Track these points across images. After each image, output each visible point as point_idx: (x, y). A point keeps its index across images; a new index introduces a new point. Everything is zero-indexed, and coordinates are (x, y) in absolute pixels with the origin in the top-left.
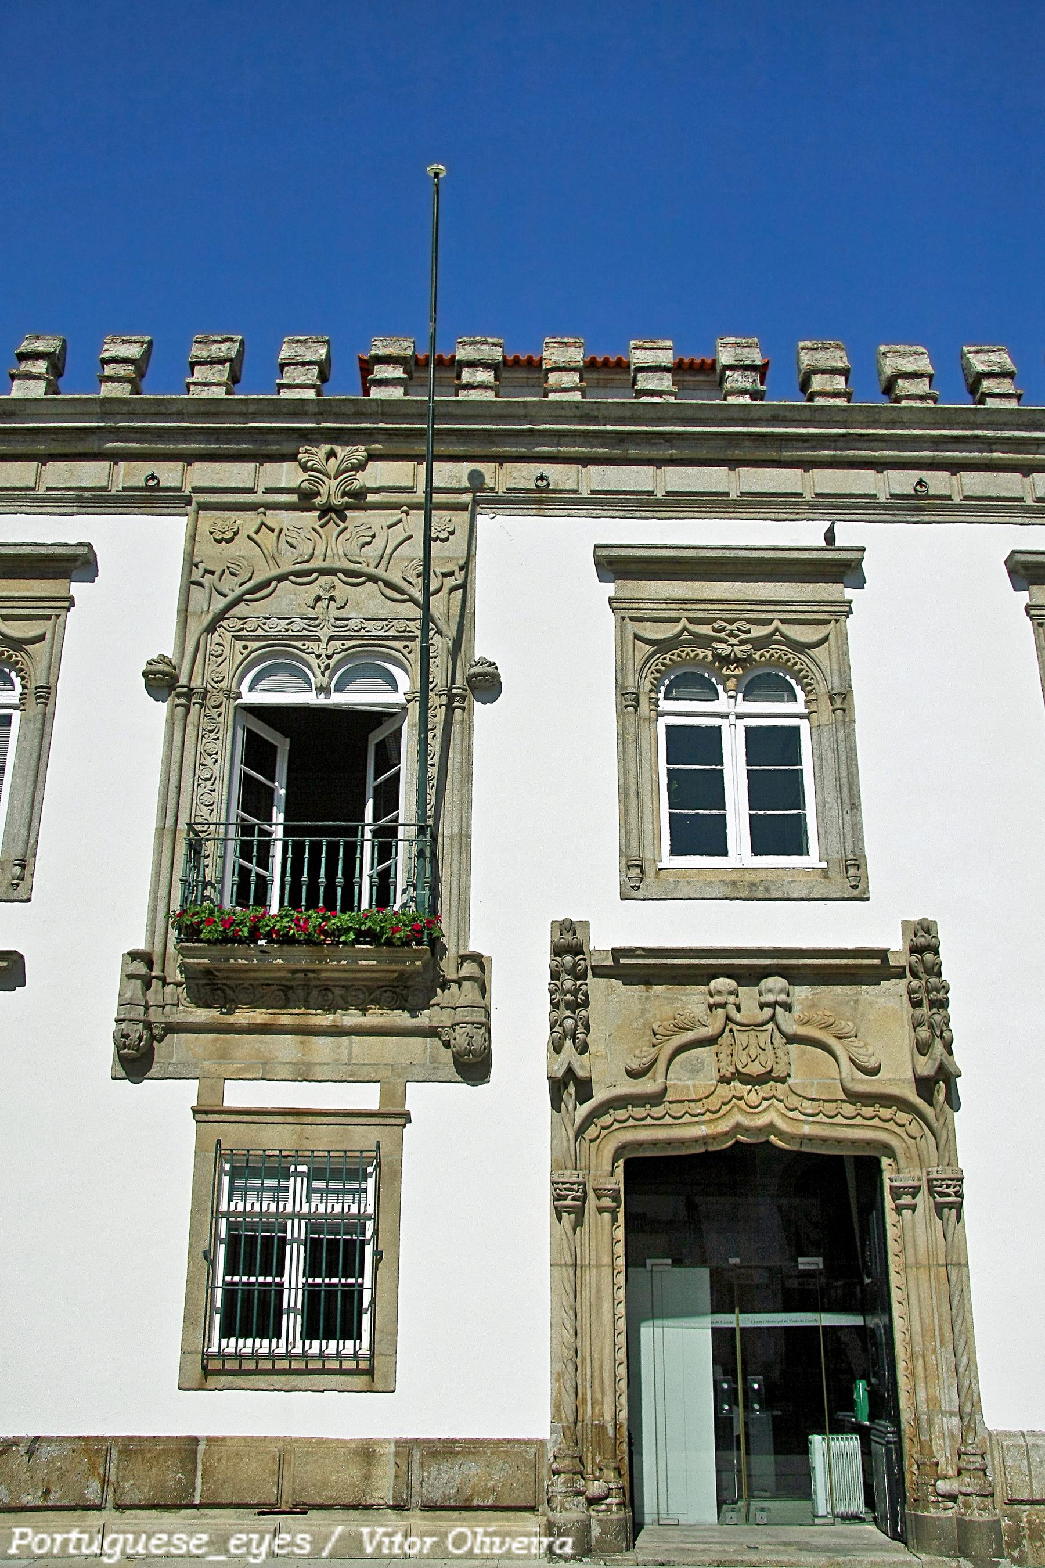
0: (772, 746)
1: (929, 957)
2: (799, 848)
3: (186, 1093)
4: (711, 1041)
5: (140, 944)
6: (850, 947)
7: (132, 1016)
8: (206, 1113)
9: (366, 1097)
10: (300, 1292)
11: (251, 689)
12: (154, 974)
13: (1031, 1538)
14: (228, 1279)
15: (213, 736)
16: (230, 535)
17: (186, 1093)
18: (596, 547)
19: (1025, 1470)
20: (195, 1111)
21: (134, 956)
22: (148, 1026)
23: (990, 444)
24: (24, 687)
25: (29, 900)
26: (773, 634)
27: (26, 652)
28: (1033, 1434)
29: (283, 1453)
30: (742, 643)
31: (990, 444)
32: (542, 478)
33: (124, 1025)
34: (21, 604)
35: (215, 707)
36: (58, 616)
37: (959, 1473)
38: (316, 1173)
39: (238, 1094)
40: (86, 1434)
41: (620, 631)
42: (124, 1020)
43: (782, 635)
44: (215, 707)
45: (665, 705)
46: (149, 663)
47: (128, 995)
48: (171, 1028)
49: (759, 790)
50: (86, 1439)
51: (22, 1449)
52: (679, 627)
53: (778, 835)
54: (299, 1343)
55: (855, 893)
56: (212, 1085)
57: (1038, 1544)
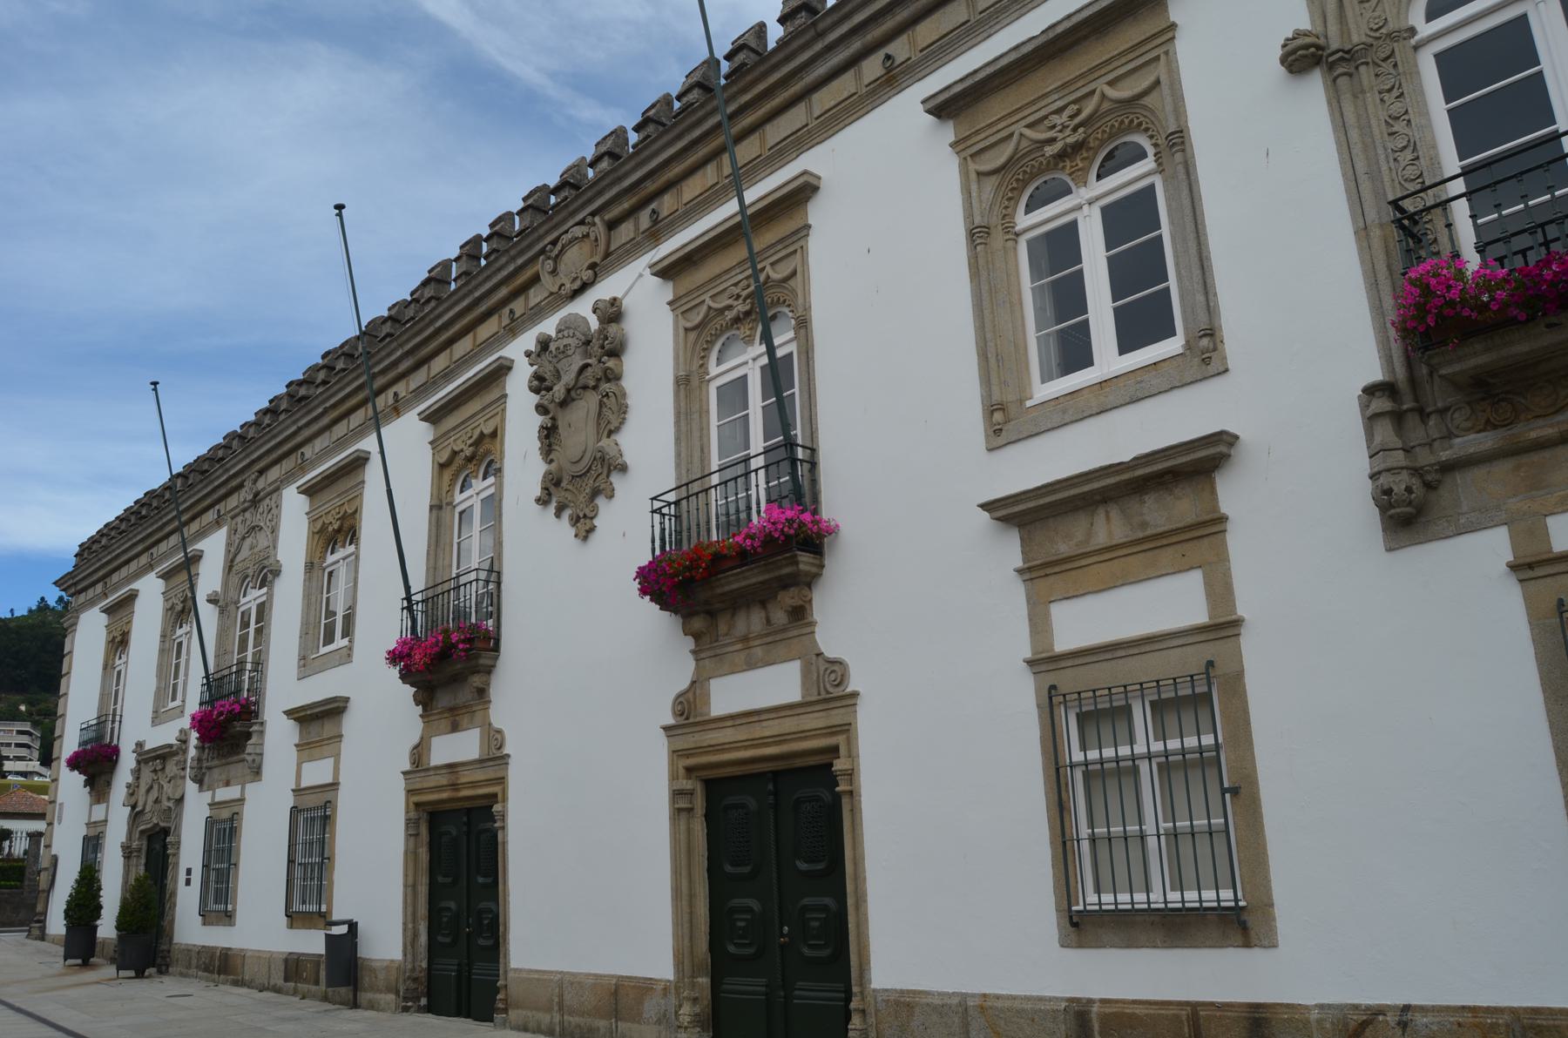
0: (1128, 218)
3: (1492, 547)
5: (1376, 374)
6: (1127, 458)
7: (1389, 464)
8: (1530, 566)
11: (719, 362)
12: (1405, 407)
15: (1395, 93)
17: (1492, 547)
20: (1514, 567)
21: (1370, 391)
22: (1416, 471)
24: (1155, 145)
25: (1227, 370)
26: (707, 315)
27: (1145, 107)
30: (1075, 130)
33: (1382, 480)
34: (983, 135)
35: (1385, 60)
36: (1167, 53)
37: (659, 1022)
38: (1158, 707)
40: (1471, 1004)
41: (964, 173)
42: (1379, 473)
44: (1385, 60)
45: (1023, 220)
46: (1284, 46)
47: (1378, 439)
48: (1448, 468)
49: (1123, 276)
50: (1474, 1010)
51: (1391, 1019)
52: (704, 308)
53: (1140, 325)
56: (1528, 530)
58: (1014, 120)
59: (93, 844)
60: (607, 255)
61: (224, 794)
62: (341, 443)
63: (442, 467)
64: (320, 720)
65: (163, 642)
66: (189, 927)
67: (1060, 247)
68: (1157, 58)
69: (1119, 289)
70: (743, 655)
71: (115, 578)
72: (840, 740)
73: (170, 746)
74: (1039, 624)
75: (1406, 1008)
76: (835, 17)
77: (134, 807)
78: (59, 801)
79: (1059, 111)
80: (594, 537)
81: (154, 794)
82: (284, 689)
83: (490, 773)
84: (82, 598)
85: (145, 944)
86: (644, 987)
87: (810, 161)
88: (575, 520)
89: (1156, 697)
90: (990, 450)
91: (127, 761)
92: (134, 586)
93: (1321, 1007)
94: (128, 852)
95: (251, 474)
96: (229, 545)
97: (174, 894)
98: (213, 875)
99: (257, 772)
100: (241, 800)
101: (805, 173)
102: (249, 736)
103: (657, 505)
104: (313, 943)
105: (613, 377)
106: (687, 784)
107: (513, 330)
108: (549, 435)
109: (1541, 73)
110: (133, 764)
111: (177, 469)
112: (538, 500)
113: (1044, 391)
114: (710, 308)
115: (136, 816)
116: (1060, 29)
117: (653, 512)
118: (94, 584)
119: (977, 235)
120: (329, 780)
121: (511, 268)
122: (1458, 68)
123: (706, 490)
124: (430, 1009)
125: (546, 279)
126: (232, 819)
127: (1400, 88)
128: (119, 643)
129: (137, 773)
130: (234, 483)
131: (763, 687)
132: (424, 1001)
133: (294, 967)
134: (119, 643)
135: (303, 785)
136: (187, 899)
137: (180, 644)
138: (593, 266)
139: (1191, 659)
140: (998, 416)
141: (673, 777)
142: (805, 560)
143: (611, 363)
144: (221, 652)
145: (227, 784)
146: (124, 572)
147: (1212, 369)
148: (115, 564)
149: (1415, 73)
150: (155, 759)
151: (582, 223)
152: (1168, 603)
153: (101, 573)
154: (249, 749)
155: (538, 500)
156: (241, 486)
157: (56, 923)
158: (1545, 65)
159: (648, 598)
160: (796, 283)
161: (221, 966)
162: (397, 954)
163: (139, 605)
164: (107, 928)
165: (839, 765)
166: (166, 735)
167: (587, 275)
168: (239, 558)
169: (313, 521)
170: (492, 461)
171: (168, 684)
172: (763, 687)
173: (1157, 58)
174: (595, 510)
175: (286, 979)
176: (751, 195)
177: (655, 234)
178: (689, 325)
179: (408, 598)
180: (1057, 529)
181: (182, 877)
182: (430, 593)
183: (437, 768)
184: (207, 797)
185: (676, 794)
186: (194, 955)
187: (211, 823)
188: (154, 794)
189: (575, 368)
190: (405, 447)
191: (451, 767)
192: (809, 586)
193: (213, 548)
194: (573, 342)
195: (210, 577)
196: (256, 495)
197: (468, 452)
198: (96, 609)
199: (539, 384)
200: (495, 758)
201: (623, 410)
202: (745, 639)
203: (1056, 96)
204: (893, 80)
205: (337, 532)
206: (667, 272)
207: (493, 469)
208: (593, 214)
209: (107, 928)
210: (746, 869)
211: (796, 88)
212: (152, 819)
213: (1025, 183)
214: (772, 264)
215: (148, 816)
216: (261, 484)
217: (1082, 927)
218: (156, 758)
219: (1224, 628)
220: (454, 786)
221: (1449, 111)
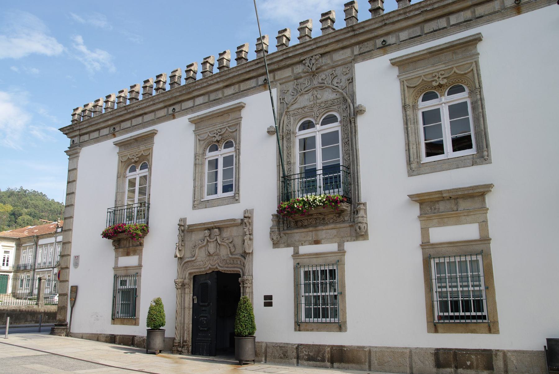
0: (457, 110)
2: (470, 147)
9: (333, 247)
17: (291, 250)
18: (390, 60)
32: (384, 41)
39: (305, 249)
43: (425, 81)
58: (424, 71)
62: (467, 23)
67: (431, 117)
68: (472, 63)
74: (425, 232)
75: (299, 345)
78: (73, 253)
87: (483, 29)
89: (459, 260)
93: (332, 347)
101: (154, 130)
103: (109, 210)
109: (441, 124)
113: (207, 198)
122: (130, 181)
127: (124, 182)
139: (333, 259)
149: (294, 142)
152: (467, 231)
158: (442, 122)
172: (130, 261)
173: (472, 63)
180: (432, 206)
183: (121, 268)
203: (462, 60)
204: (385, 47)
210: (206, 304)
213: (128, 166)
217: (299, 326)
219: (140, 266)
221: (223, 170)
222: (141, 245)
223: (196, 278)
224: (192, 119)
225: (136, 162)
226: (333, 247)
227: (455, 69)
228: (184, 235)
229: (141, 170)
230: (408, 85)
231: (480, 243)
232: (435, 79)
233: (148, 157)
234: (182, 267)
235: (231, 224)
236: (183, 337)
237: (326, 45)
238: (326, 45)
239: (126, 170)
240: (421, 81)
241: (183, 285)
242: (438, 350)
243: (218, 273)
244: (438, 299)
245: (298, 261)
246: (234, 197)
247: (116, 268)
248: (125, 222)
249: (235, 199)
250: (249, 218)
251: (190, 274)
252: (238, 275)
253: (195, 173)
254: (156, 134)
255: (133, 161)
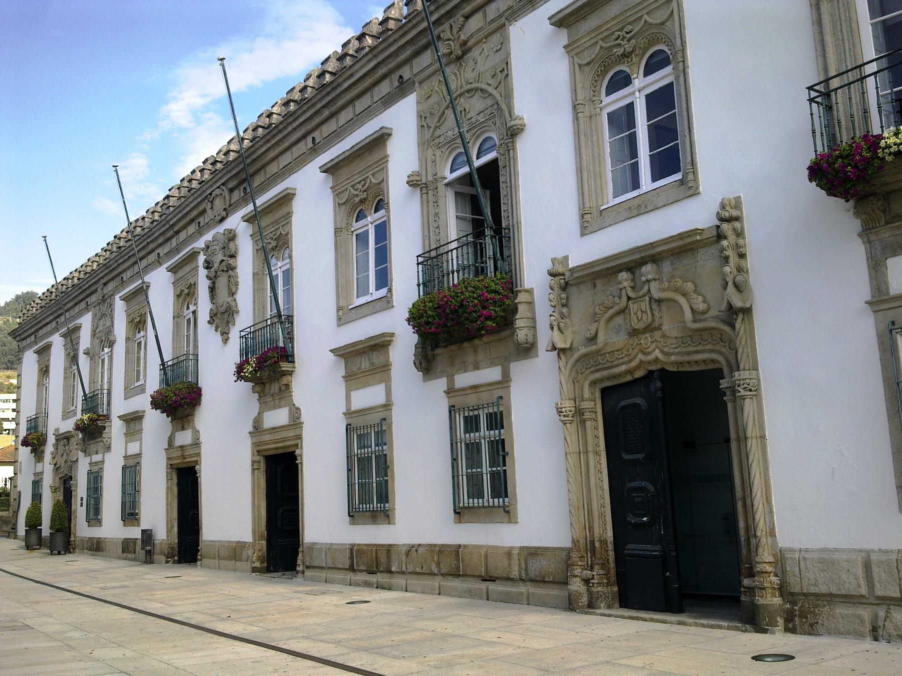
1: (737, 224)
4: (622, 311)
9: (492, 374)
10: (465, 477)
13: (801, 616)
14: (469, 471)
16: (499, 46)
18: (549, 19)
19: (797, 573)
23: (395, 54)
28: (807, 550)
29: (488, 553)
31: (395, 54)
45: (607, 100)
54: (491, 500)
55: (691, 192)
57: (804, 620)
59: (37, 484)
60: (230, 205)
61: (96, 458)
63: (179, 296)
64: (133, 420)
65: (65, 373)
66: (82, 529)
67: (623, 120)
69: (654, 143)
70: (272, 403)
71: (41, 333)
72: (299, 441)
73: (70, 432)
76: (233, 165)
77: (55, 465)
79: (359, 183)
80: (230, 341)
81: (65, 457)
82: (120, 406)
83: (291, 433)
84: (24, 343)
85: (61, 540)
86: (242, 545)
88: (222, 334)
90: (338, 326)
91: (51, 440)
92: (78, 321)
94: (54, 490)
95: (99, 285)
96: (93, 322)
97: (76, 511)
98: (92, 500)
99: (108, 448)
100: (103, 462)
101: (287, 189)
102: (104, 428)
104: (135, 533)
105: (233, 268)
106: (257, 458)
107: (200, 232)
108: (212, 289)
110: (54, 441)
111: (132, 219)
112: (209, 322)
114: (601, 47)
115: (57, 468)
116: (356, 148)
117: (418, 264)
118: (29, 336)
119: (338, 231)
120: (138, 452)
121: (196, 202)
123: (862, 79)
124: (179, 562)
125: (209, 211)
126: (135, 466)
128: (44, 371)
129: (56, 446)
130: (93, 288)
131: (278, 417)
132: (176, 558)
133: (127, 546)
134: (44, 371)
135: (129, 454)
136: (80, 512)
137: (140, 343)
138: (225, 210)
140: (341, 312)
141: (253, 455)
142: (285, 366)
143: (231, 261)
144: (93, 381)
145: (97, 453)
146: (44, 331)
147: (390, 305)
148: (40, 325)
150: (64, 439)
151: (219, 187)
153: (33, 330)
154: (104, 435)
155: (209, 322)
156: (96, 291)
157: (22, 529)
159: (814, 183)
160: (384, 185)
161: (96, 547)
162: (165, 537)
163: (152, 294)
164: (46, 529)
165: (197, 467)
166: (68, 426)
167: (224, 214)
168: (98, 330)
169: (128, 316)
170: (381, 200)
171: (69, 398)
172: (278, 417)
174: (229, 330)
175: (123, 552)
176: (251, 207)
177: (315, 150)
178: (341, 202)
179: (163, 363)
181: (79, 502)
182: (175, 361)
184: (88, 459)
185: (253, 462)
186: (85, 543)
187: (90, 473)
188: (65, 457)
189: (219, 260)
190: (160, 284)
191: (181, 447)
192: (291, 375)
193: (86, 322)
194: (217, 248)
195: (85, 340)
196: (103, 297)
197: (186, 291)
198: (163, 268)
199: (208, 265)
200: (296, 422)
201: (237, 284)
202: (272, 395)
205: (138, 323)
206: (330, 169)
207: (381, 204)
208: (223, 184)
209: (46, 529)
211: (286, 144)
212: (64, 471)
214: (373, 175)
215: (62, 470)
216: (105, 291)
218: (65, 438)
220: (184, 457)
222: (288, 386)
223: (609, 394)
224: (325, 168)
225: (363, 201)
226: (492, 374)
227: (646, 17)
228: (567, 299)
229: (645, 75)
230: (580, 62)
231: (470, 391)
232: (618, 41)
233: (382, 185)
234: (571, 370)
235: (685, 246)
236: (591, 528)
237: (44, 319)
238: (44, 319)
239: (595, 92)
240: (598, 48)
241: (579, 412)
242: (353, 545)
243: (663, 373)
244: (489, 469)
245: (891, 315)
246: (682, 182)
247: (349, 414)
248: (876, 131)
249: (689, 189)
250: (737, 219)
251: (593, 383)
252: (718, 374)
253: (254, 298)
254: (390, 135)
255: (357, 200)
